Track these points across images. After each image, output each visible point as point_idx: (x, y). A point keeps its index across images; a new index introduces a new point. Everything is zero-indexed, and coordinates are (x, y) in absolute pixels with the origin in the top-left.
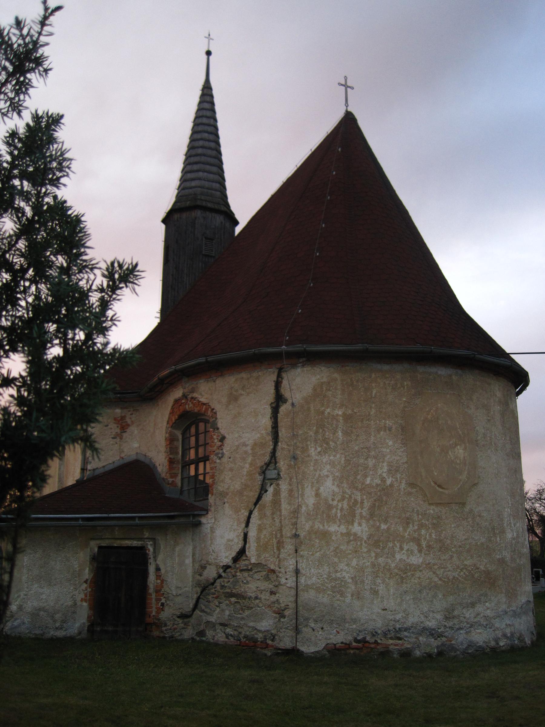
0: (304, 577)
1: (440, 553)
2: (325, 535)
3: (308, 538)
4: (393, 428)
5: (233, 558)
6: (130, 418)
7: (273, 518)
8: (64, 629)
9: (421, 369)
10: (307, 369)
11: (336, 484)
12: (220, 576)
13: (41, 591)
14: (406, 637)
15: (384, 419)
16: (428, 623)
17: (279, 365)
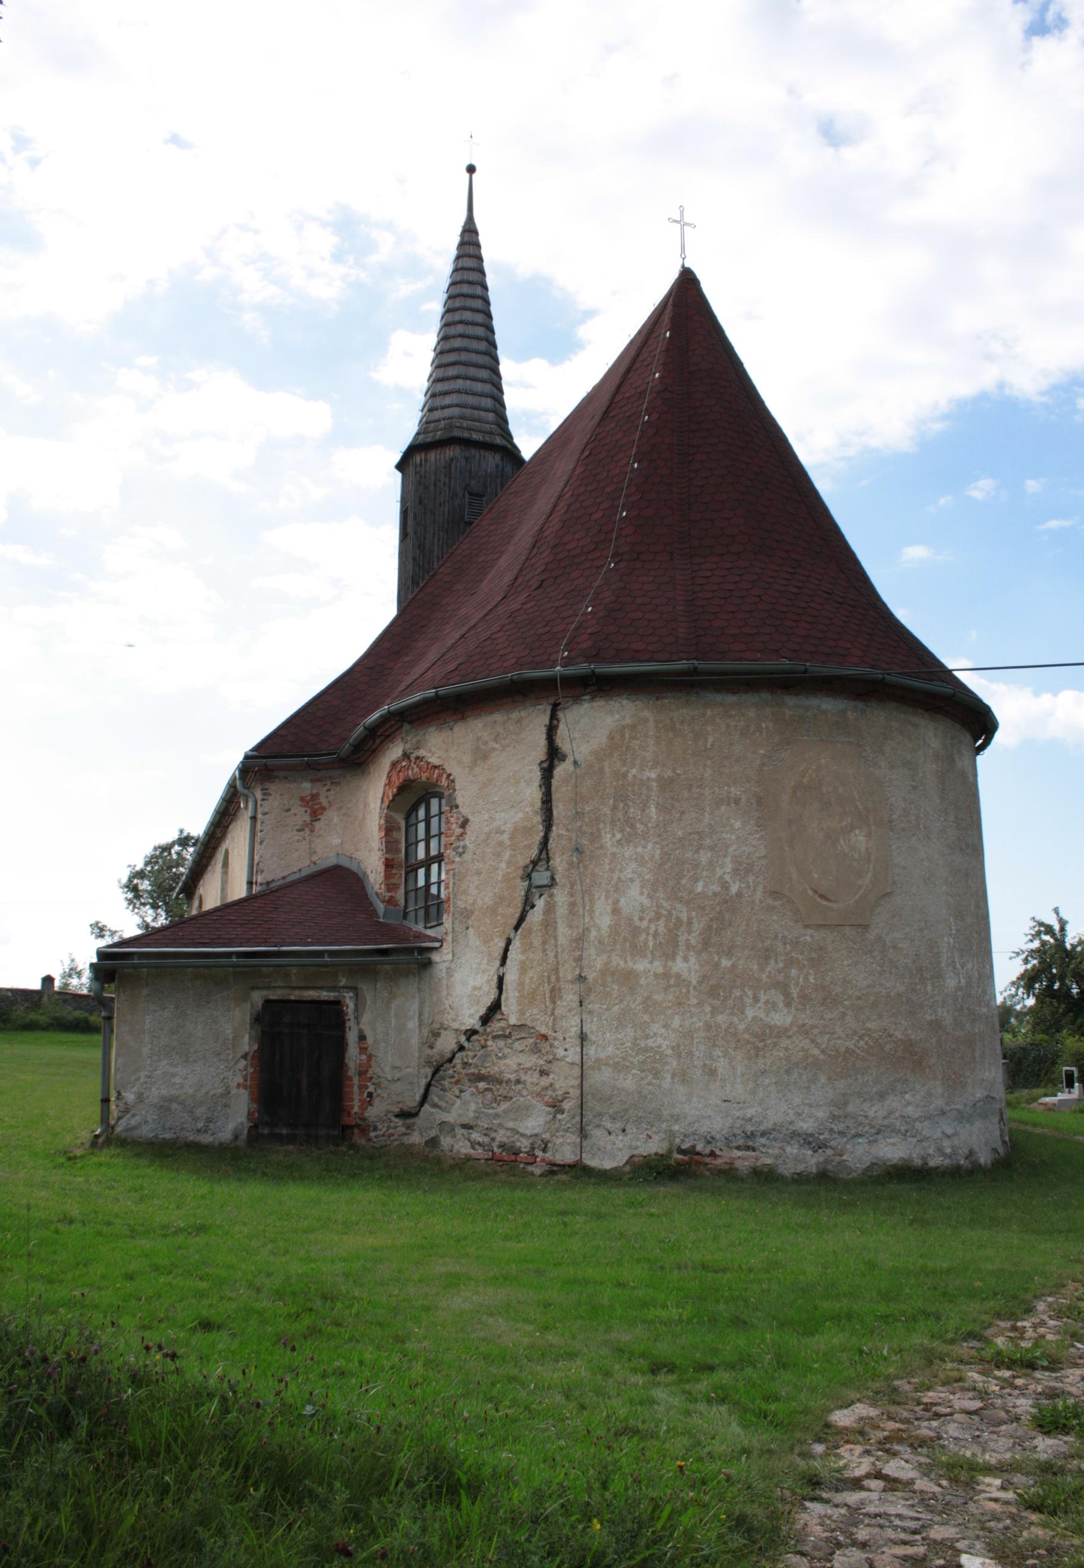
0: (594, 1046)
1: (822, 1008)
2: (629, 978)
3: (600, 981)
4: (743, 800)
5: (481, 1017)
6: (327, 797)
7: (545, 951)
8: (210, 1132)
9: (791, 700)
10: (600, 703)
11: (646, 892)
12: (461, 1048)
13: (172, 1070)
14: (764, 1146)
15: (727, 785)
16: (801, 1124)
17: (552, 700)
